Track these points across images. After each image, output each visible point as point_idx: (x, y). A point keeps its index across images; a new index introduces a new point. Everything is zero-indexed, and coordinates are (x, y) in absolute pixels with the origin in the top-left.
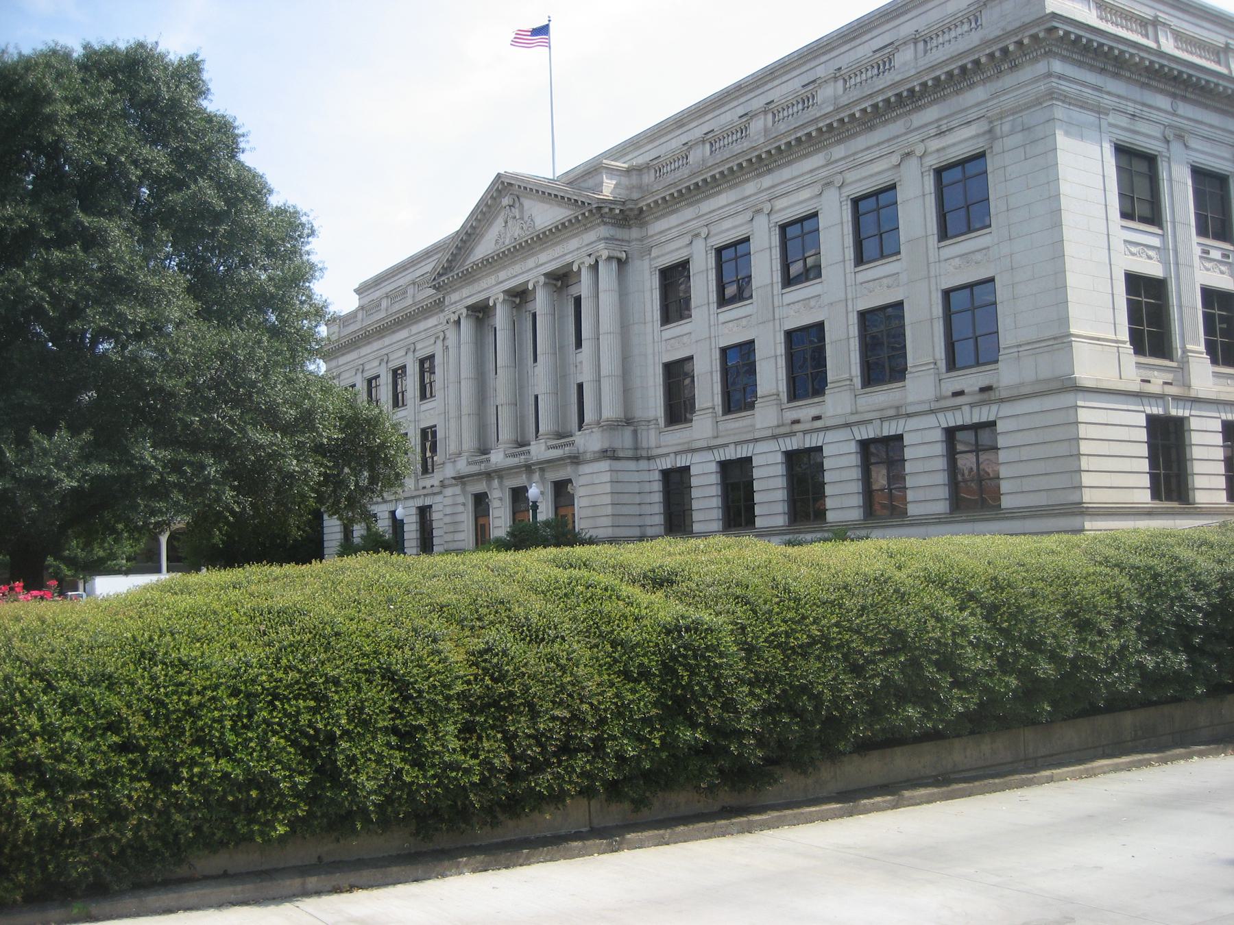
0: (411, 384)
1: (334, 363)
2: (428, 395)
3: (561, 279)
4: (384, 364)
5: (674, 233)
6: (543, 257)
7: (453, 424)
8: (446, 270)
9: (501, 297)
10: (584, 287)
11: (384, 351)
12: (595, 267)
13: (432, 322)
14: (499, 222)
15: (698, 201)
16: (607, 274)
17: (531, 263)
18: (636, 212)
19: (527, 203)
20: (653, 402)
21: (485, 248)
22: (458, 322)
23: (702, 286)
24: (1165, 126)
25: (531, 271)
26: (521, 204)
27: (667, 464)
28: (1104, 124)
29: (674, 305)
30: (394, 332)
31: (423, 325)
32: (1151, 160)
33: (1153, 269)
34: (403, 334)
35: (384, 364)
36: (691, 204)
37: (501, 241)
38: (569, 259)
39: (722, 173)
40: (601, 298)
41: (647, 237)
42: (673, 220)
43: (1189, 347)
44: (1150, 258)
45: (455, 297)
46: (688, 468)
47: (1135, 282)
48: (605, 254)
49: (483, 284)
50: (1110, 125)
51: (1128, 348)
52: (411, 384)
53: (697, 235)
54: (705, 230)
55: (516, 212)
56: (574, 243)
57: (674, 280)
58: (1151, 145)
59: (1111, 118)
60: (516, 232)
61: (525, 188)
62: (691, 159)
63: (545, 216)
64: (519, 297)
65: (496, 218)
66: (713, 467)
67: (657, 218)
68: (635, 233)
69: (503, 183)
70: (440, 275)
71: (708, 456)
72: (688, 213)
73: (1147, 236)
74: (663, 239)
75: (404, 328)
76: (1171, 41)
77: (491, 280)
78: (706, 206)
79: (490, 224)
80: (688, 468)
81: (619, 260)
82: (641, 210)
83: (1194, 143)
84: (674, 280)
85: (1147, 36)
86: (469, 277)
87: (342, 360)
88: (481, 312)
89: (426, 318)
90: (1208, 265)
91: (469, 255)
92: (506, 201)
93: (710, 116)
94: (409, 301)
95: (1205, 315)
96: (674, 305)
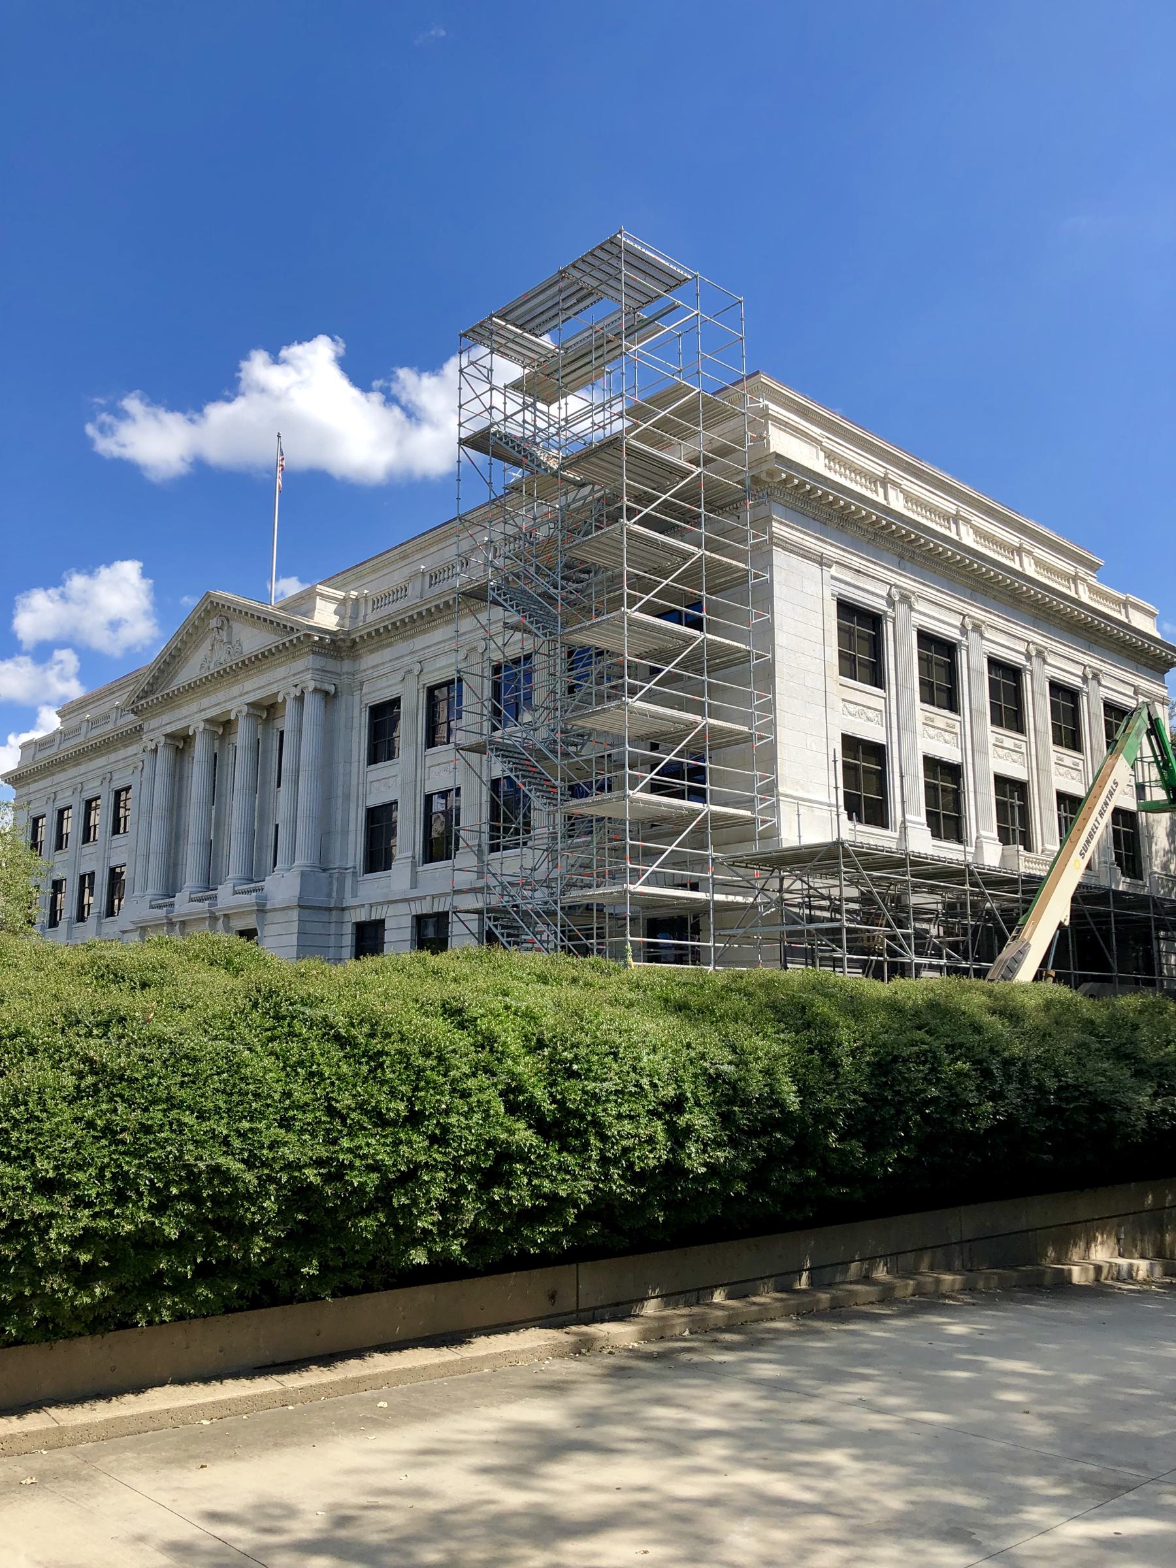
0: (101, 818)
1: (24, 790)
2: (122, 831)
3: (266, 711)
4: (77, 794)
5: (386, 669)
6: (248, 685)
7: (140, 862)
8: (146, 694)
9: (202, 725)
10: (287, 722)
11: (79, 780)
12: (300, 699)
13: (131, 750)
14: (207, 645)
15: (413, 636)
16: (312, 705)
17: (236, 690)
18: (348, 644)
19: (236, 626)
20: (354, 848)
21: (190, 671)
22: (155, 751)
23: (410, 727)
24: (1085, 667)
25: (234, 699)
26: (230, 627)
27: (362, 916)
28: (827, 575)
29: (381, 746)
30: (91, 760)
31: (122, 753)
32: (874, 620)
33: (873, 733)
34: (100, 762)
35: (77, 794)
36: (404, 639)
37: (206, 665)
38: (274, 689)
39: (437, 607)
40: (302, 733)
41: (359, 671)
42: (386, 654)
43: (983, 833)
44: (869, 719)
45: (154, 723)
46: (382, 922)
47: (851, 744)
48: (311, 685)
49: (184, 711)
50: (833, 578)
51: (844, 815)
52: (101, 818)
53: (410, 672)
54: (417, 667)
55: (224, 634)
56: (281, 672)
57: (383, 718)
58: (952, 633)
59: (834, 570)
60: (223, 658)
61: (240, 611)
62: (409, 591)
63: (252, 640)
64: (223, 727)
65: (203, 640)
66: (407, 922)
67: (372, 651)
68: (347, 666)
69: (212, 602)
70: (139, 698)
71: (403, 908)
72: (401, 647)
73: (868, 695)
74: (376, 674)
75: (103, 755)
76: (1033, 566)
77: (194, 707)
78: (420, 642)
79: (197, 647)
80: (382, 922)
81: (327, 693)
82: (354, 642)
83: (919, 606)
84: (383, 718)
85: (1069, 588)
86: (170, 701)
87: (34, 787)
88: (181, 743)
89: (126, 746)
90: (932, 731)
91: (172, 679)
92: (214, 623)
93: (435, 548)
94: (110, 726)
95: (999, 804)
96: (381, 746)
